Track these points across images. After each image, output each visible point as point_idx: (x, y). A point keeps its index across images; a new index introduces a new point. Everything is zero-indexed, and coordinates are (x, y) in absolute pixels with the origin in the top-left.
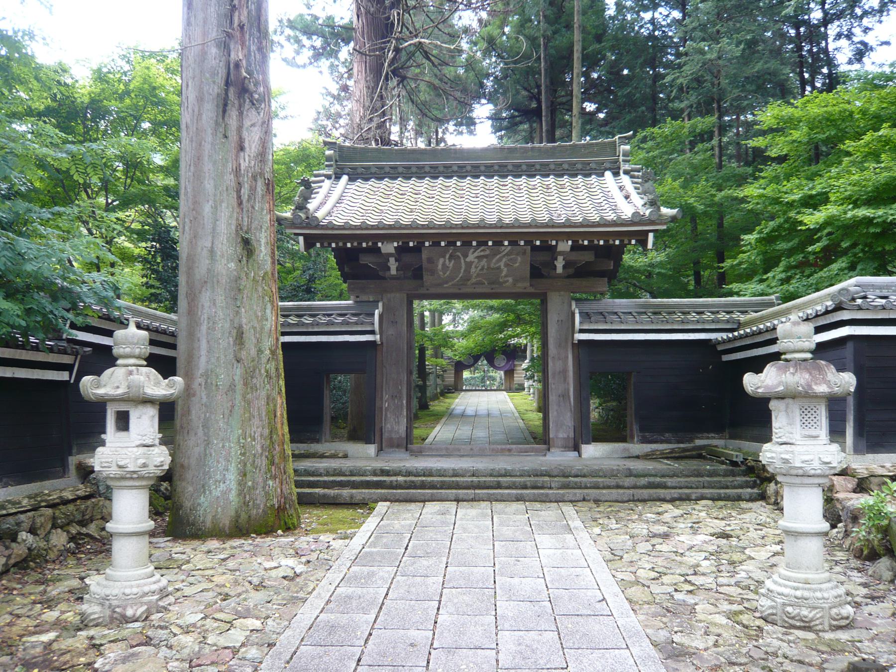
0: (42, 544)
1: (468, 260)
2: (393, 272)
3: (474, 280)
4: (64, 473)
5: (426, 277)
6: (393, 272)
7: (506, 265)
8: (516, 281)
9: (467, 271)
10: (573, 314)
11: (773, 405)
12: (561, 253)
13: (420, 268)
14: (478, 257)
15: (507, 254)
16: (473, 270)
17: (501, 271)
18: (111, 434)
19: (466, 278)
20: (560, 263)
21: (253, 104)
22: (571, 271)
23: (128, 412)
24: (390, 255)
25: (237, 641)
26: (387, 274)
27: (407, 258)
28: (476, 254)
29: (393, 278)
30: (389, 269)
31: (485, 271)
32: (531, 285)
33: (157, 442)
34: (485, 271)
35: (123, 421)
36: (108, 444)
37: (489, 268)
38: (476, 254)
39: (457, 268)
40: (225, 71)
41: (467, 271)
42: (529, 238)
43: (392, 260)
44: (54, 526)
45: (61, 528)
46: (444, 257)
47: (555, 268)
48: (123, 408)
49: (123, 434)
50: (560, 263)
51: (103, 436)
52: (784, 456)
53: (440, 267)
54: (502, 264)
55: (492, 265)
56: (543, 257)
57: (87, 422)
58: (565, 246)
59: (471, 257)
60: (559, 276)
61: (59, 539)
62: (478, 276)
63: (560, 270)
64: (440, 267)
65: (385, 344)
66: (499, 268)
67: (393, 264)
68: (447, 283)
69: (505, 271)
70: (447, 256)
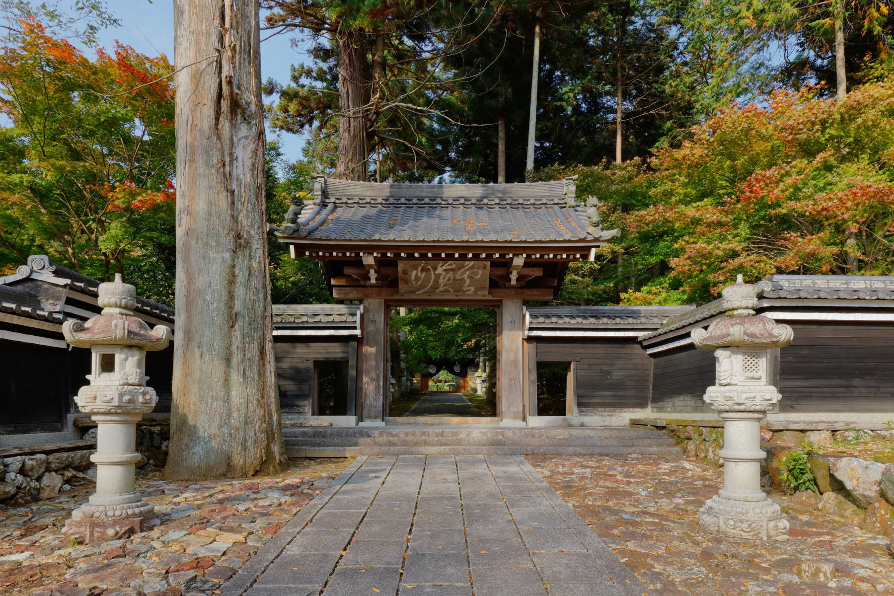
0: (34, 484)
1: (437, 272)
2: (373, 281)
3: (441, 289)
4: (62, 426)
5: (402, 287)
6: (373, 281)
7: (470, 277)
8: (477, 290)
9: (436, 281)
10: (524, 316)
11: (719, 353)
12: (516, 267)
13: (397, 279)
14: (445, 270)
15: (470, 268)
16: (441, 280)
17: (465, 282)
18: (96, 377)
19: (436, 286)
20: (514, 276)
21: (245, 119)
22: (523, 283)
23: (113, 355)
24: (371, 266)
25: (219, 551)
26: (368, 283)
27: (385, 271)
28: (444, 268)
29: (372, 286)
30: (369, 279)
31: (451, 282)
32: (489, 293)
33: (144, 384)
34: (451, 282)
35: (108, 365)
36: (92, 383)
37: (454, 279)
38: (444, 268)
39: (427, 280)
40: (216, 85)
41: (436, 281)
42: (490, 249)
43: (372, 272)
44: (48, 470)
45: (56, 471)
46: (417, 269)
47: (510, 280)
48: (108, 351)
49: (106, 375)
50: (514, 276)
51: (88, 377)
52: (727, 394)
53: (413, 277)
54: (466, 276)
55: (457, 277)
56: (500, 272)
57: (75, 366)
58: (519, 261)
59: (440, 270)
60: (513, 287)
61: (53, 481)
62: (445, 285)
63: (513, 282)
64: (413, 277)
65: (365, 339)
66: (463, 279)
67: (373, 274)
68: (419, 290)
69: (468, 281)
70: (420, 269)
